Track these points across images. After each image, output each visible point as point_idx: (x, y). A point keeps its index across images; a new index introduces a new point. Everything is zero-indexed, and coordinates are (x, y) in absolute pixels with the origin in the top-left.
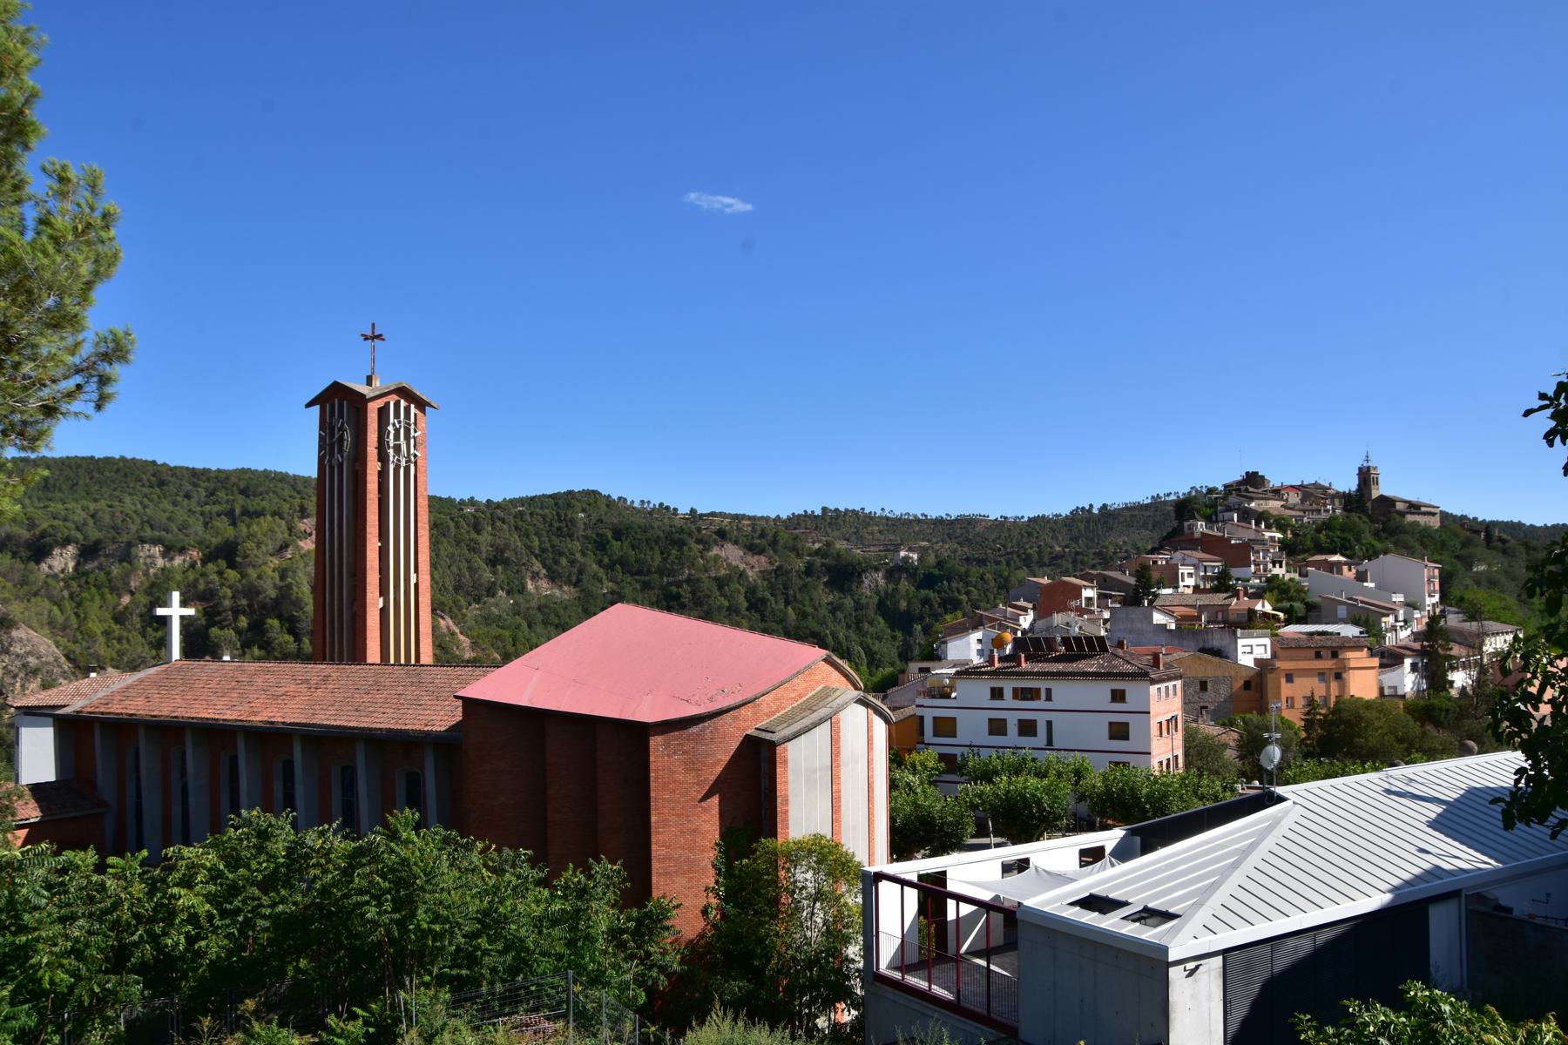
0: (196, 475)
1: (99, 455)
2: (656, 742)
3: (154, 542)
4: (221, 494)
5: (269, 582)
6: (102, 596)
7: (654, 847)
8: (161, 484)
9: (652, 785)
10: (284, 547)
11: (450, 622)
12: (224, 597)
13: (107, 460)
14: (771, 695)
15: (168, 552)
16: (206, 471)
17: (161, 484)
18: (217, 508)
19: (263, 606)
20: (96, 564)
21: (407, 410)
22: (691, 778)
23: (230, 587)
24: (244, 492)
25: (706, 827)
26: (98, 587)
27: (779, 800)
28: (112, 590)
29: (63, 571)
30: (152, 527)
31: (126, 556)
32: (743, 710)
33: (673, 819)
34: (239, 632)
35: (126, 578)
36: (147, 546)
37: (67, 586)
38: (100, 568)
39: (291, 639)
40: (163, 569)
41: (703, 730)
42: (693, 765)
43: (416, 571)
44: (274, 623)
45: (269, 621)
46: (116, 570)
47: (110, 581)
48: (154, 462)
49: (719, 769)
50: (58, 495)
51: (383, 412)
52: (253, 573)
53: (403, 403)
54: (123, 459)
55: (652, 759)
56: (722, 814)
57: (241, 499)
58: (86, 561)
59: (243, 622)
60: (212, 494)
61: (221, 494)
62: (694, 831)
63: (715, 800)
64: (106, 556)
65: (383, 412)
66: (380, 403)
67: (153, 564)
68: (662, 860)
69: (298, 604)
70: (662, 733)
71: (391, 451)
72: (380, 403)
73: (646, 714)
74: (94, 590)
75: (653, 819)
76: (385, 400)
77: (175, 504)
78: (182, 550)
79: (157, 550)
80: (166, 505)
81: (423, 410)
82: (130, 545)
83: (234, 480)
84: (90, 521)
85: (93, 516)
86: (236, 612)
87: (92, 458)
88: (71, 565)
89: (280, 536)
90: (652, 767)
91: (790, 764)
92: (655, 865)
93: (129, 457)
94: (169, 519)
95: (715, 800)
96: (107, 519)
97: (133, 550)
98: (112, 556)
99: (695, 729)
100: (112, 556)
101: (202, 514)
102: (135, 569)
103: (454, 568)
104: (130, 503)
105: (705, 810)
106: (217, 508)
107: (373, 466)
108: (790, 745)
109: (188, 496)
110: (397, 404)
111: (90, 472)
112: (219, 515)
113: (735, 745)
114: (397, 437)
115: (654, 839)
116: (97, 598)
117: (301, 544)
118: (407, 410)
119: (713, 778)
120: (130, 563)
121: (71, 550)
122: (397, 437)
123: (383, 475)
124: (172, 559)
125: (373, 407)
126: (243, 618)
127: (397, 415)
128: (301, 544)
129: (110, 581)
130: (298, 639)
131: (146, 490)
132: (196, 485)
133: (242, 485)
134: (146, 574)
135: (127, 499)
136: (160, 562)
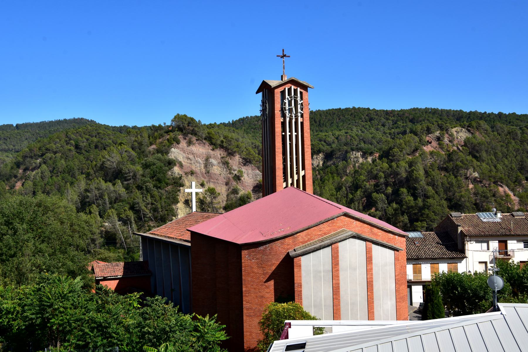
0: (387, 113)
1: (343, 107)
2: (244, 253)
3: (358, 150)
4: (400, 123)
5: (403, 169)
6: (333, 178)
7: (244, 303)
8: (371, 119)
9: (243, 273)
10: (416, 150)
11: (507, 189)
12: (381, 177)
13: (347, 109)
14: (305, 233)
15: (364, 156)
16: (393, 111)
17: (371, 119)
18: (397, 130)
19: (401, 182)
20: (332, 162)
21: (295, 91)
22: (260, 271)
23: (383, 172)
24: (412, 121)
25: (267, 295)
26: (332, 174)
27: (296, 285)
28: (338, 174)
29: (318, 166)
30: (365, 142)
31: (345, 158)
32: (287, 240)
33: (253, 290)
34: (386, 195)
35: (345, 167)
36: (354, 152)
37: (319, 173)
38: (334, 164)
39: (412, 198)
40: (362, 164)
41: (266, 249)
42: (261, 265)
43: (303, 168)
44: (404, 190)
45: (402, 189)
46: (341, 164)
47: (337, 170)
48: (368, 109)
49: (274, 268)
50: (325, 128)
51: (283, 93)
52: (394, 164)
53: (299, 89)
54: (354, 108)
55: (243, 261)
56: (275, 289)
57: (410, 125)
58: (327, 161)
59: (390, 190)
60: (396, 123)
61: (400, 123)
62: (262, 297)
63: (272, 283)
64: (336, 158)
65: (283, 93)
66: (281, 89)
67: (358, 161)
68: (247, 309)
69: (416, 180)
70: (247, 249)
71: (287, 112)
72: (281, 89)
73: (240, 242)
74: (330, 175)
75: (244, 289)
76: (284, 87)
77: (377, 129)
78: (371, 154)
79: (359, 154)
80: (373, 130)
81: (306, 90)
82: (347, 152)
83: (407, 115)
84: (336, 141)
85: (337, 138)
86: (387, 184)
87: (340, 109)
88: (321, 163)
89: (413, 145)
90: (243, 265)
91: (303, 268)
92: (245, 311)
93: (357, 107)
94: (372, 138)
95: (272, 283)
96: (343, 139)
97: (348, 155)
98: (339, 158)
99: (262, 248)
100: (339, 158)
101: (390, 134)
102: (348, 164)
103: (519, 158)
104: (355, 131)
105: (267, 287)
106: (397, 130)
107: (278, 120)
108: (303, 258)
109: (383, 125)
110: (290, 90)
111: (339, 116)
112: (398, 134)
113: (282, 257)
114: (290, 104)
115: (244, 299)
116: (331, 179)
117: (425, 148)
118: (295, 91)
119: (270, 272)
120: (346, 161)
121: (321, 155)
122: (290, 104)
123: (283, 124)
124: (366, 158)
125: (278, 92)
126: (389, 188)
127: (290, 94)
128: (425, 148)
129: (337, 170)
130: (415, 198)
131: (363, 124)
132: (387, 119)
133: (411, 117)
134: (354, 166)
135: (355, 129)
136: (361, 160)
